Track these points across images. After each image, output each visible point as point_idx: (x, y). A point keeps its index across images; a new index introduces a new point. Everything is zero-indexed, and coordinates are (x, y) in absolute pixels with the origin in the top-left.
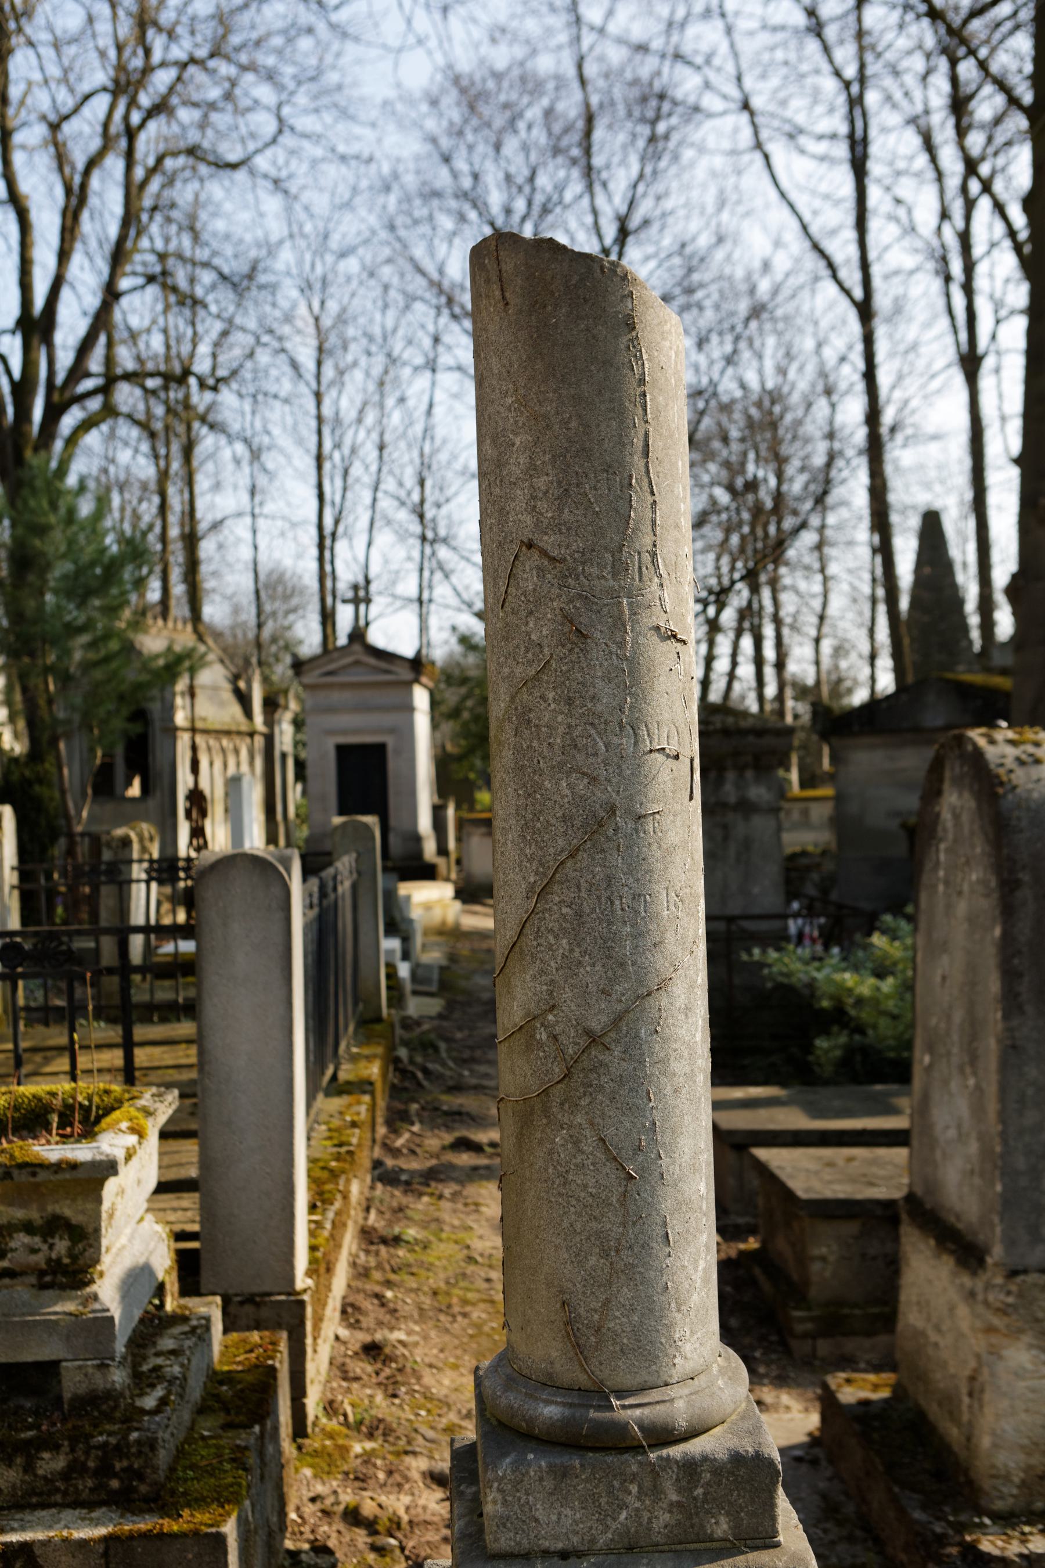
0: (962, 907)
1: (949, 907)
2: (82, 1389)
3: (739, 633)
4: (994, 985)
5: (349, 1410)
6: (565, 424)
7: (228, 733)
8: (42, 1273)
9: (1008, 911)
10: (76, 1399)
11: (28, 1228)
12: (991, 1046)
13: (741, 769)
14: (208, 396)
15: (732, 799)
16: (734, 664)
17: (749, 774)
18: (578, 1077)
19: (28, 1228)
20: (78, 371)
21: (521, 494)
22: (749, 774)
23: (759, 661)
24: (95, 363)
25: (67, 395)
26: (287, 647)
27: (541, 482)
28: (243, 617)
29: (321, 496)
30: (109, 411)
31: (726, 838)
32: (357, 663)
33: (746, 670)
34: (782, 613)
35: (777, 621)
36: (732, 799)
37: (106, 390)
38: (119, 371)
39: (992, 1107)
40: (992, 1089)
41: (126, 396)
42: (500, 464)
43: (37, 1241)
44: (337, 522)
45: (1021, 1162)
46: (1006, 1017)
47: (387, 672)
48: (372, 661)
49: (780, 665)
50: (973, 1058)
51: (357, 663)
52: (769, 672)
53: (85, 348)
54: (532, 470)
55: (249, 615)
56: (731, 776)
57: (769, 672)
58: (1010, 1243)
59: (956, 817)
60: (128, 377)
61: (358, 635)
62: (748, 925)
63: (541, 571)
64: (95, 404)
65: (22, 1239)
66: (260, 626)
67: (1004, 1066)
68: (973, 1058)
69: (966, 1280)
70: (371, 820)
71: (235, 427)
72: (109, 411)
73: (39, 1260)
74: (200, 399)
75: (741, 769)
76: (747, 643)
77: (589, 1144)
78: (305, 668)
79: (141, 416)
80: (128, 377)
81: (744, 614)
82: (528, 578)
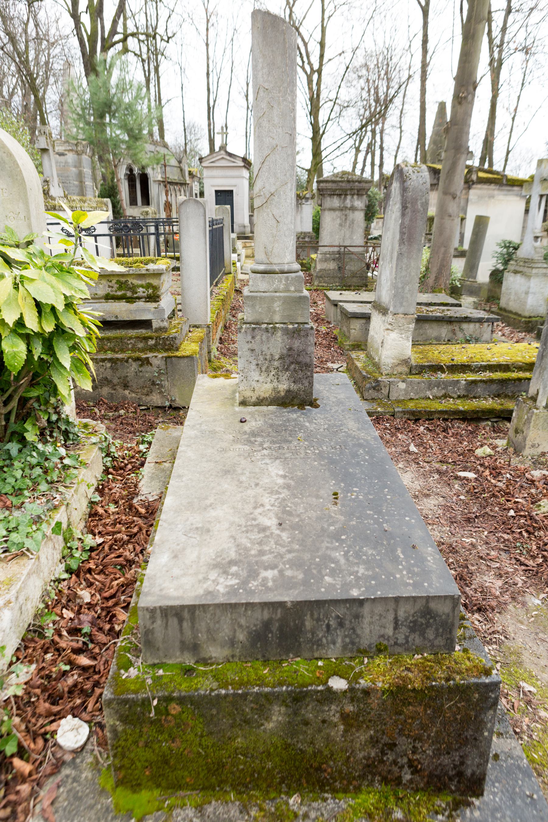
0: (394, 216)
1: (391, 217)
2: (158, 326)
3: (367, 153)
4: (398, 237)
5: (220, 429)
6: (270, 57)
7: (176, 184)
8: (146, 298)
9: (403, 215)
10: (156, 328)
11: (142, 286)
12: (395, 254)
13: (353, 195)
14: (164, 44)
15: (349, 206)
16: (364, 165)
17: (355, 197)
18: (269, 202)
19: (142, 286)
20: (113, 32)
21: (260, 74)
22: (355, 197)
23: (373, 164)
24: (120, 29)
25: (109, 43)
26: (197, 153)
27: (264, 71)
28: (179, 141)
29: (209, 90)
30: (126, 50)
31: (346, 219)
32: (223, 158)
33: (368, 168)
34: (384, 145)
35: (382, 148)
36: (349, 206)
37: (124, 40)
38: (129, 32)
39: (394, 270)
40: (394, 266)
41: (132, 43)
42: (256, 66)
43: (144, 290)
44: (215, 101)
45: (400, 285)
46: (399, 246)
47: (234, 162)
48: (228, 158)
49: (381, 165)
50: (392, 258)
51: (223, 158)
52: (377, 169)
53: (115, 22)
54: (263, 68)
55: (182, 141)
56: (349, 197)
57: (377, 169)
58: (395, 307)
59: (395, 189)
60: (133, 35)
61: (223, 148)
62: (351, 249)
63: (264, 92)
64: (119, 46)
65: (141, 289)
66: (186, 144)
67: (398, 259)
68: (392, 258)
69: (383, 318)
70: (228, 207)
71: (175, 59)
72: (126, 50)
73: (145, 294)
74: (161, 45)
75: (353, 195)
76: (369, 156)
77: (271, 215)
78: (203, 160)
79: (138, 52)
80: (133, 35)
81: (369, 146)
82: (261, 94)
